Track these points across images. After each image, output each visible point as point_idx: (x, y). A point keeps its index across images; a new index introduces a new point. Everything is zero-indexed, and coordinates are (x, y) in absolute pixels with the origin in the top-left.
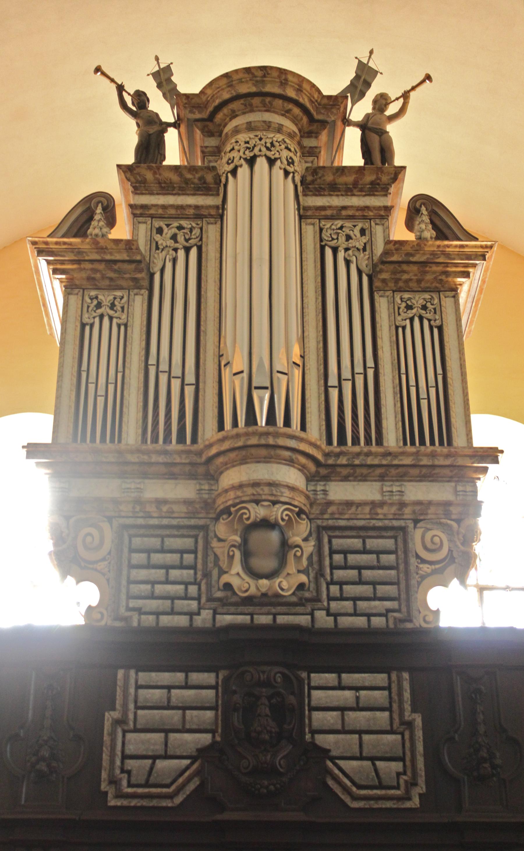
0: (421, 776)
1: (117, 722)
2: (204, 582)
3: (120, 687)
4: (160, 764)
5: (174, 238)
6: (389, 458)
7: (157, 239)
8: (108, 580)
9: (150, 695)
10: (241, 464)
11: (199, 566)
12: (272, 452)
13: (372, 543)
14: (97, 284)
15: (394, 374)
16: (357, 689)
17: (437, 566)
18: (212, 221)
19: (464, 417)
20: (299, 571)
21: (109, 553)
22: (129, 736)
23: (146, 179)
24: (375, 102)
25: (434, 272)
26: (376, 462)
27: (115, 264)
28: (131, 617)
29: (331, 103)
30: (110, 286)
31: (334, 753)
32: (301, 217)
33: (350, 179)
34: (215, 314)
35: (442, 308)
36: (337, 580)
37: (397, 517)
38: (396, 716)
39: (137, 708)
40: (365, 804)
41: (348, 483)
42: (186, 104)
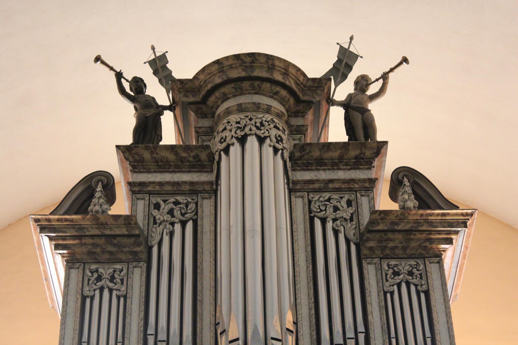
7: (154, 215)
18: (206, 196)
23: (144, 158)
25: (418, 240)
27: (115, 239)
29: (316, 85)
30: (109, 259)
32: (290, 191)
42: (180, 88)
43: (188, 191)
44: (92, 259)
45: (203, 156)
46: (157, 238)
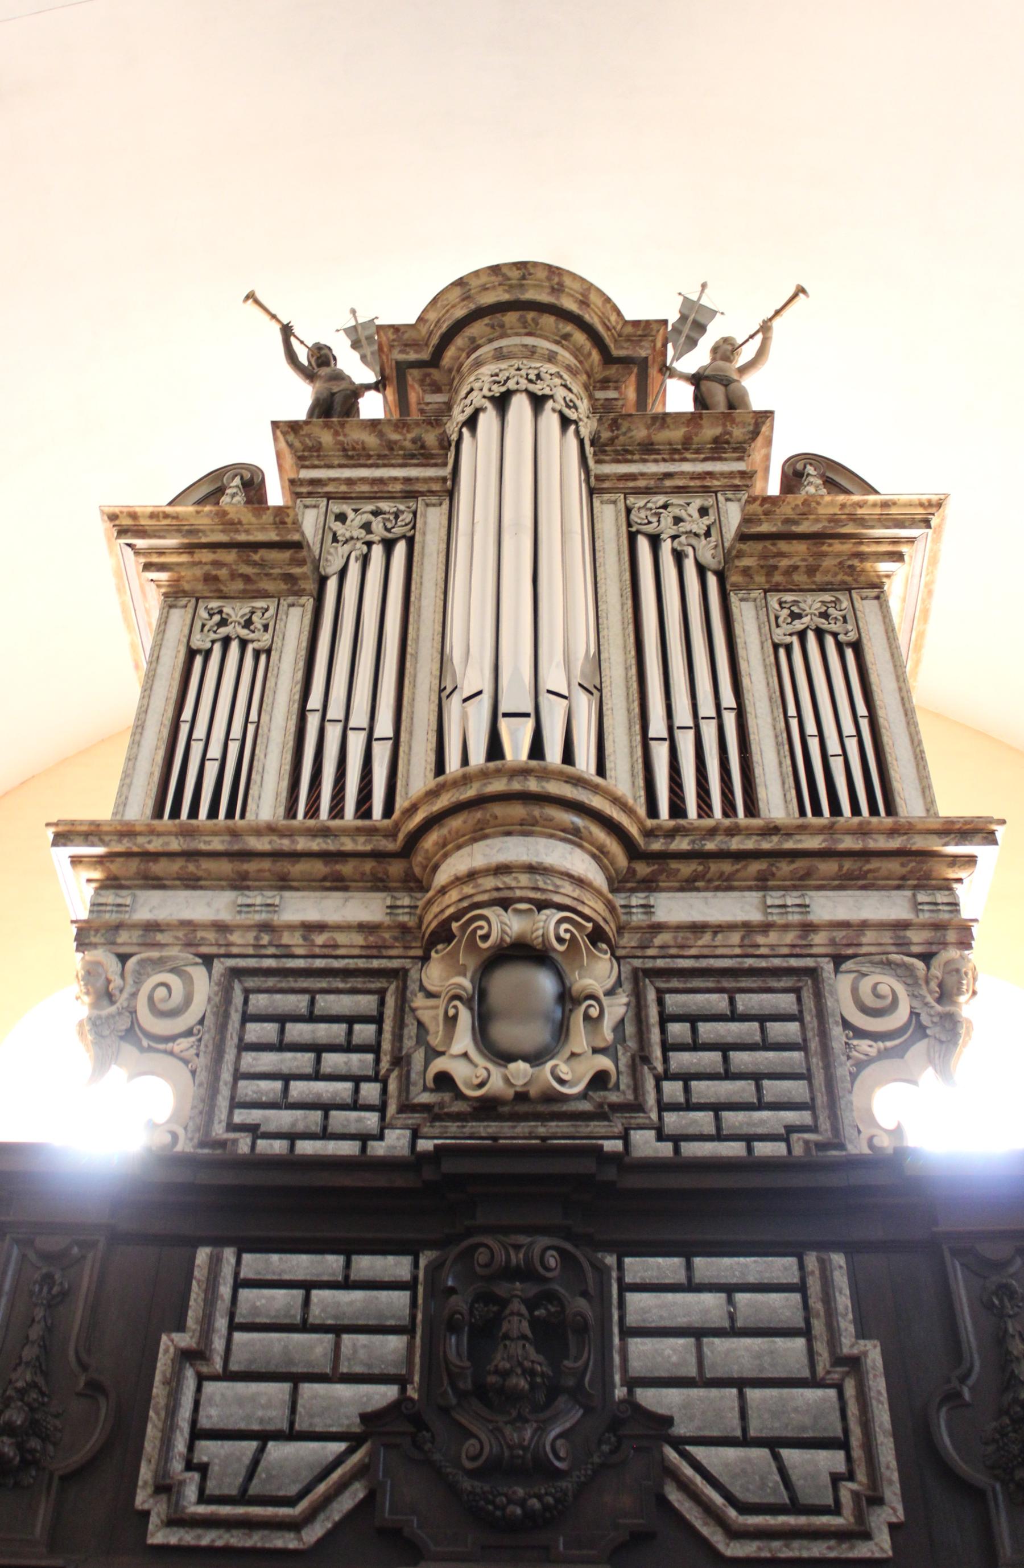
0: (891, 1482)
1: (187, 1356)
2: (394, 1075)
3: (199, 1281)
4: (276, 1451)
5: (367, 527)
6: (775, 839)
7: (334, 529)
8: (193, 1073)
9: (263, 1301)
10: (475, 840)
11: (386, 1046)
12: (536, 811)
14: (223, 588)
15: (776, 714)
16: (730, 1290)
17: (889, 1044)
18: (434, 501)
19: (917, 782)
20: (596, 1051)
21: (201, 1022)
22: (209, 1387)
23: (320, 443)
24: (715, 350)
25: (838, 555)
26: (749, 844)
27: (256, 552)
28: (235, 1141)
29: (639, 333)
30: (244, 591)
31: (681, 1429)
32: (591, 492)
33: (676, 434)
34: (434, 630)
35: (858, 613)
36: (677, 1071)
38: (821, 1348)
39: (233, 1326)
40: (760, 1549)
41: (694, 894)
42: (394, 340)
43: (400, 492)
44: (211, 591)
46: (337, 565)
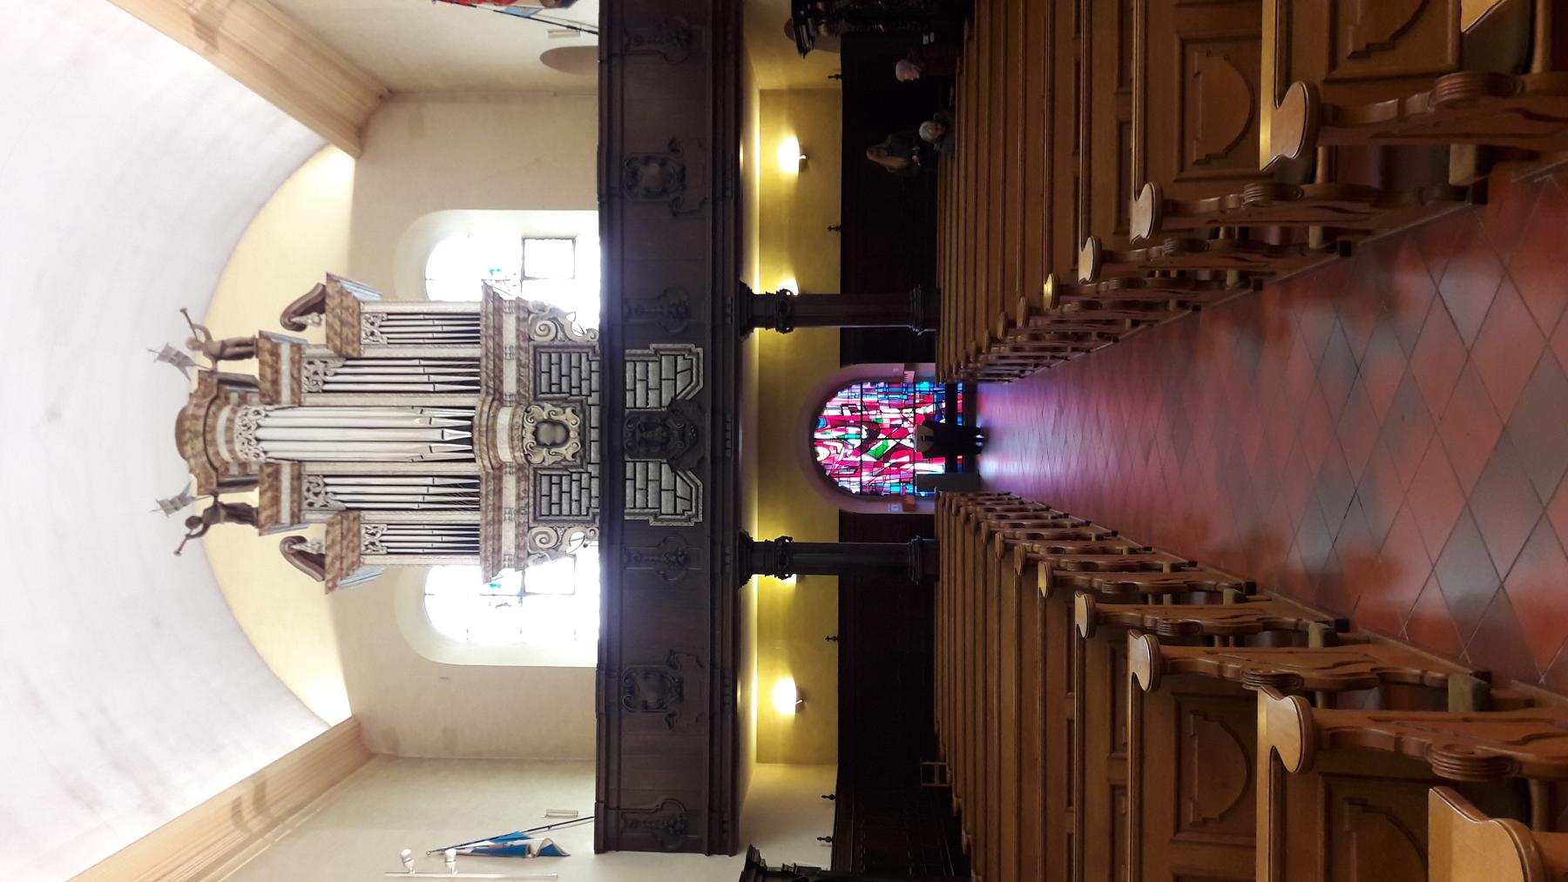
1: (656, 519)
4: (679, 493)
5: (316, 494)
13: (544, 367)
24: (194, 348)
33: (268, 371)
37: (527, 351)
45: (269, 470)
